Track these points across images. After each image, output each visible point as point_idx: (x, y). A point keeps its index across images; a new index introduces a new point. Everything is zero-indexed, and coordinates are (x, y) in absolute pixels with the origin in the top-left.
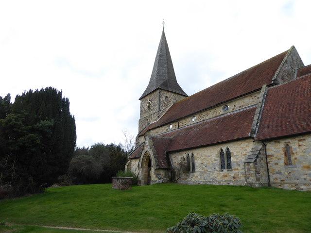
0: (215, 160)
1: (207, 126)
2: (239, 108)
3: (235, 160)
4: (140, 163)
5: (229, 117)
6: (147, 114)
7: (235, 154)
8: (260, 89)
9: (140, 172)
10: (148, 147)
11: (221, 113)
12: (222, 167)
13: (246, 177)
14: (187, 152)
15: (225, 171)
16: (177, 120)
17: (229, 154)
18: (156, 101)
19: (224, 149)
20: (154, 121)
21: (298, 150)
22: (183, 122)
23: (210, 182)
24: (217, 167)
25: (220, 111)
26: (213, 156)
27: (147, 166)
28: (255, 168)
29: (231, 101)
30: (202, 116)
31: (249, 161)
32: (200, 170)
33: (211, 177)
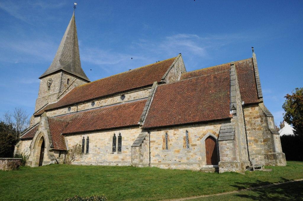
0: (108, 144)
1: (104, 112)
2: (133, 99)
3: (125, 144)
4: (33, 144)
5: (124, 106)
6: (46, 94)
7: (125, 139)
8: (151, 85)
9: (32, 153)
10: (43, 128)
11: (118, 101)
12: (114, 150)
13: (133, 159)
14: (83, 136)
15: (116, 153)
16: (77, 104)
17: (120, 138)
18: (59, 80)
19: (117, 133)
20: (53, 101)
21: (173, 137)
22: (83, 105)
23: (101, 163)
24: (109, 150)
25: (117, 99)
26: (106, 139)
27: (40, 148)
28: (140, 151)
29: (98, 99)
30: (101, 102)
31: (135, 145)
32: (94, 152)
33: (103, 158)
